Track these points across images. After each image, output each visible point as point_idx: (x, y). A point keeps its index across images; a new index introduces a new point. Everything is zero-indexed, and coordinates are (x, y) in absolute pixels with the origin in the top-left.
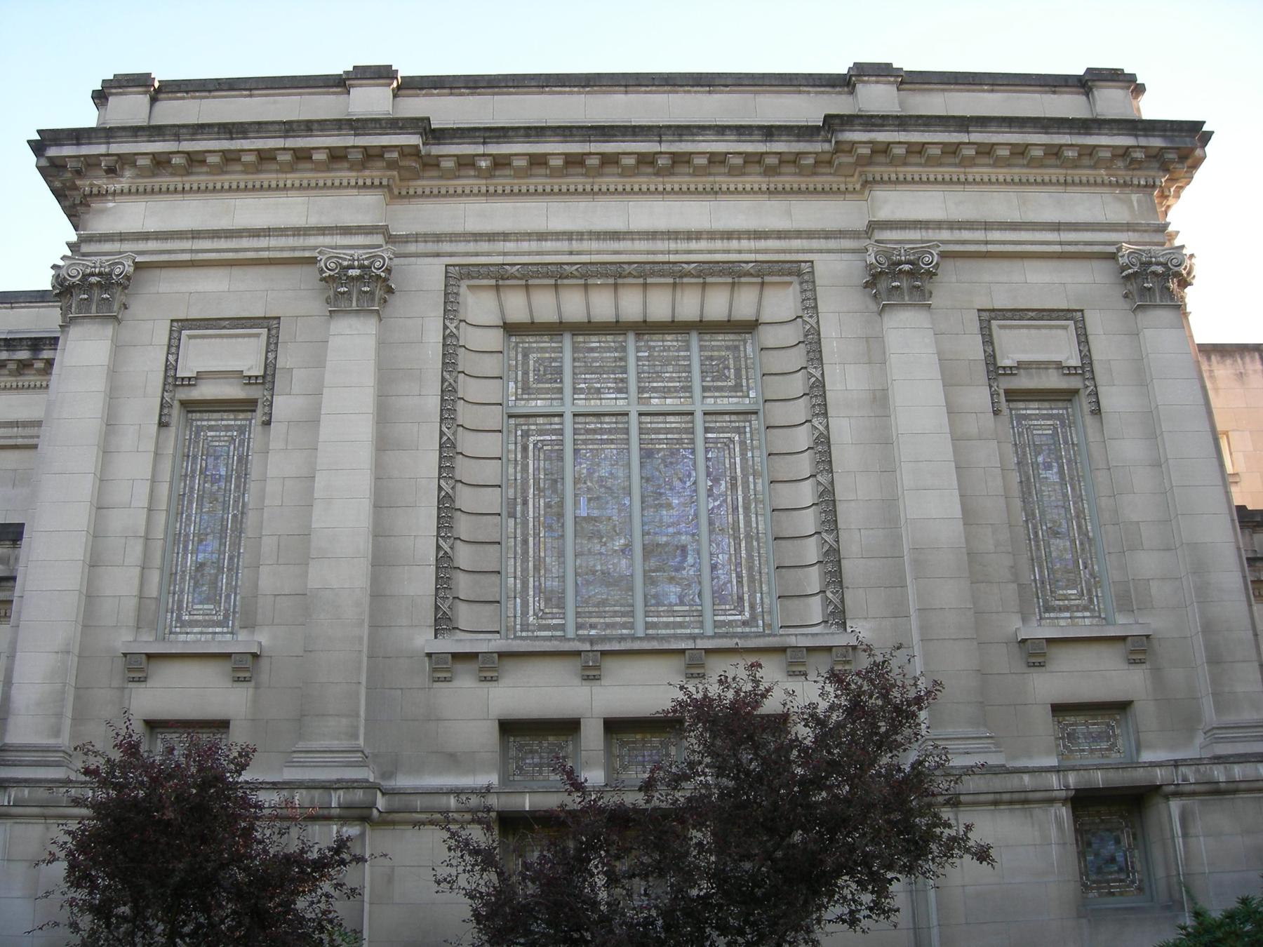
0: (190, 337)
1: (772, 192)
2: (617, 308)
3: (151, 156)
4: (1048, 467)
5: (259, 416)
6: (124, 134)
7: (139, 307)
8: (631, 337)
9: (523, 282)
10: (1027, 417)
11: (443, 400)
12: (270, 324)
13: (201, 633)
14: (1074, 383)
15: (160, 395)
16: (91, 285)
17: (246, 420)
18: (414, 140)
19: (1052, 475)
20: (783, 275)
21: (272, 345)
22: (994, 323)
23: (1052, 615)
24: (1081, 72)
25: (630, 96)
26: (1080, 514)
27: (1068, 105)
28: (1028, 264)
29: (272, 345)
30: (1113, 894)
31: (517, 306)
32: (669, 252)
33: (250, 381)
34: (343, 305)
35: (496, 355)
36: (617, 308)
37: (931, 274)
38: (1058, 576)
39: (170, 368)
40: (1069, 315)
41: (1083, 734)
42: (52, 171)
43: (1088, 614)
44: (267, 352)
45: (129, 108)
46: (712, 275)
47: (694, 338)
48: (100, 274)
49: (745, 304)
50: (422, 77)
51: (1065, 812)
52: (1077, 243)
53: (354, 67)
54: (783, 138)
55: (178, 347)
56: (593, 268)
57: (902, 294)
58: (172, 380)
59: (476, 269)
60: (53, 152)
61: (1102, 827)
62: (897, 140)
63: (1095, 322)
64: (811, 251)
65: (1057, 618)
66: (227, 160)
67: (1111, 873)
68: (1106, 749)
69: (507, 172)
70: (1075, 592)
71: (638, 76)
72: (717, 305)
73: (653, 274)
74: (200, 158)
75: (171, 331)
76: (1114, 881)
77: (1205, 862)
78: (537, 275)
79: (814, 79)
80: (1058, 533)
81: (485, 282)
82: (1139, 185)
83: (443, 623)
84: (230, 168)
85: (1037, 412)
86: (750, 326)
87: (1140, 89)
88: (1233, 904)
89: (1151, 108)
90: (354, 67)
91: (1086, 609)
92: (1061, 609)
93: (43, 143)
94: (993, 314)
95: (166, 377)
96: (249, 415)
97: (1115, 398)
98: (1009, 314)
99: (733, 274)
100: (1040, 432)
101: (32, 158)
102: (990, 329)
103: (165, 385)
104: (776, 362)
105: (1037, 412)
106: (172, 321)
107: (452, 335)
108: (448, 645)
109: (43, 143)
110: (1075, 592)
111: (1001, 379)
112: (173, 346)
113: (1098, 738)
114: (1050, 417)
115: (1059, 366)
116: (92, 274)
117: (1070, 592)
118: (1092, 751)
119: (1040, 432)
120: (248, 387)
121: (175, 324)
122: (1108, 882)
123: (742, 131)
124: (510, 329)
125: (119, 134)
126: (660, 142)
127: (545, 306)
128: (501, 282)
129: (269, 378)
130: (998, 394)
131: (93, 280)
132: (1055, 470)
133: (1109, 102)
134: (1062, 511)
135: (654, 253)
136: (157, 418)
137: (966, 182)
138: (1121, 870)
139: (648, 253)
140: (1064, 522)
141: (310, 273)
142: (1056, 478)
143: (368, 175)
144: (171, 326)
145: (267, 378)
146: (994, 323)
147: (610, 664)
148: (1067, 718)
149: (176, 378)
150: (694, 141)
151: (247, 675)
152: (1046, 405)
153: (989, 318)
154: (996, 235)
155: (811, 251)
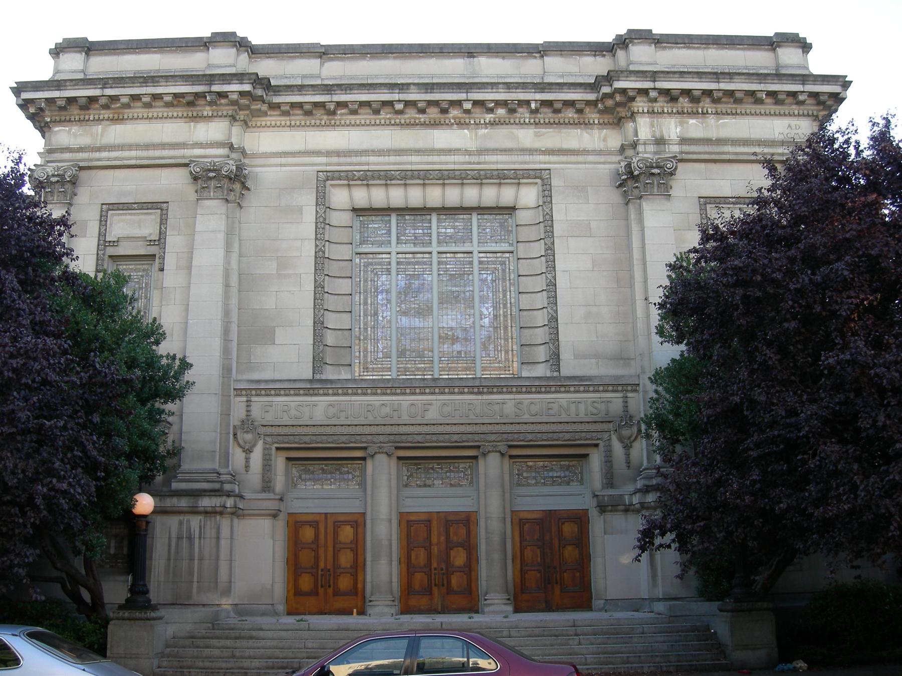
2: (424, 197)
6: (662, 75)
12: (159, 207)
14: (153, 250)
18: (247, 87)
21: (163, 221)
24: (771, 34)
27: (760, 60)
29: (163, 221)
31: (361, 196)
33: (151, 243)
34: (205, 194)
36: (424, 197)
39: (102, 235)
42: (24, 105)
45: (73, 63)
47: (475, 217)
48: (58, 175)
49: (507, 196)
54: (775, 82)
55: (106, 221)
57: (209, 192)
60: (25, 95)
63: (173, 212)
64: (550, 163)
66: (155, 99)
71: (173, 41)
72: (490, 195)
74: (224, 94)
75: (102, 211)
79: (727, 40)
81: (438, 182)
86: (511, 210)
87: (806, 47)
89: (818, 63)
93: (19, 89)
94: (111, 207)
95: (99, 240)
97: (170, 261)
99: (501, 177)
101: (13, 98)
103: (98, 245)
104: (524, 233)
109: (19, 89)
112: (103, 221)
121: (104, 206)
123: (700, 75)
124: (357, 211)
126: (803, 84)
127: (378, 196)
128: (389, 182)
129: (162, 241)
131: (54, 179)
133: (789, 56)
137: (736, 114)
139: (522, 163)
141: (183, 172)
144: (102, 208)
149: (105, 241)
155: (550, 163)
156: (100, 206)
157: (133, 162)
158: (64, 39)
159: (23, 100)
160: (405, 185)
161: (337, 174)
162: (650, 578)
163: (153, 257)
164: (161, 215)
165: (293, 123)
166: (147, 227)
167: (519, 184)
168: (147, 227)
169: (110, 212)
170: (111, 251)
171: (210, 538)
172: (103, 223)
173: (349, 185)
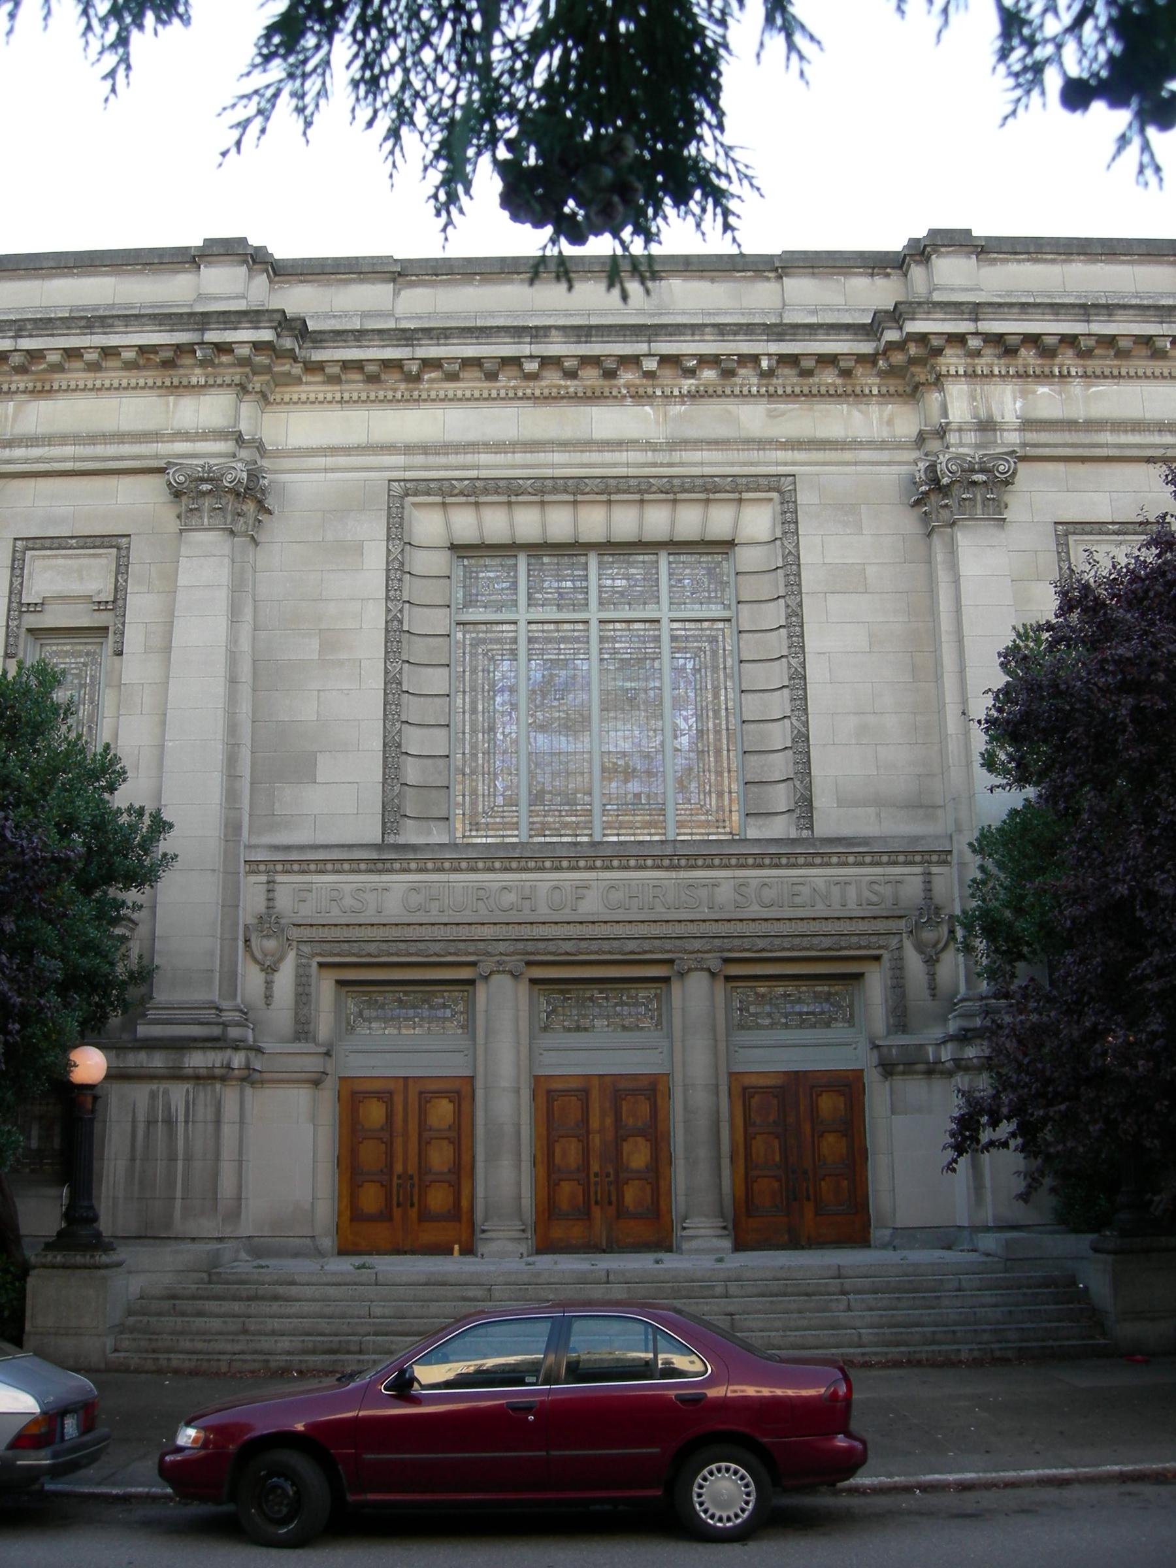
6: (990, 310)
8: (522, 562)
9: (736, 496)
15: (4, 624)
18: (266, 335)
21: (122, 569)
22: (1071, 538)
29: (122, 569)
33: (101, 606)
35: (442, 580)
37: (1007, 483)
39: (15, 593)
47: (663, 559)
50: (1086, 239)
53: (205, 240)
55: (22, 569)
59: (744, 480)
63: (139, 552)
73: (486, 491)
75: (14, 551)
77: (160, 1124)
78: (555, 490)
82: (957, 375)
86: (728, 545)
90: (205, 240)
94: (1071, 528)
95: (10, 602)
98: (98, 542)
102: (1067, 545)
103: (9, 611)
106: (16, 539)
111: (26, 616)
112: (17, 568)
120: (96, 613)
121: (19, 543)
123: (1056, 309)
124: (458, 549)
125: (1030, 311)
128: (513, 499)
129: (120, 603)
144: (14, 546)
145: (117, 603)
146: (1071, 538)
149: (21, 604)
150: (52, 335)
153: (1067, 530)
157: (69, 466)
161: (423, 485)
164: (118, 558)
167: (740, 500)
170: (31, 621)
172: (18, 572)
173: (444, 504)
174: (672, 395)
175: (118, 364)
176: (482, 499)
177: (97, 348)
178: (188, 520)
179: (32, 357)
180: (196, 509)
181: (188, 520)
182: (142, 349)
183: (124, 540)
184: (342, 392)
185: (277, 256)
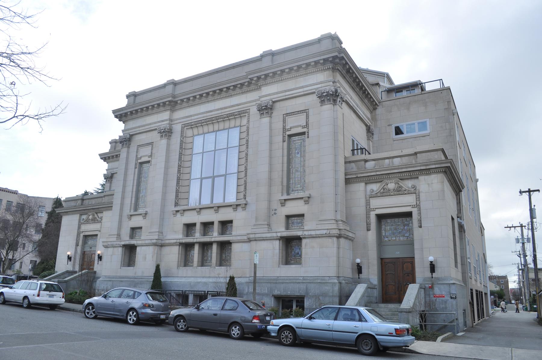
0: (288, 118)
1: (243, 93)
3: (297, 66)
4: (298, 153)
5: (306, 136)
7: (275, 113)
10: (295, 141)
11: (179, 156)
12: (151, 144)
13: (142, 209)
16: (263, 109)
17: (304, 137)
19: (299, 156)
20: (244, 113)
21: (307, 117)
23: (294, 192)
25: (218, 74)
26: (304, 166)
28: (297, 99)
29: (307, 117)
30: (297, 262)
32: (221, 113)
38: (296, 182)
40: (305, 111)
41: (296, 222)
43: (302, 191)
44: (306, 119)
46: (230, 117)
51: (120, 249)
52: (307, 91)
56: (208, 120)
57: (264, 115)
58: (284, 130)
61: (297, 245)
62: (302, 63)
63: (311, 112)
65: (294, 193)
67: (297, 257)
68: (301, 226)
69: (311, 67)
70: (299, 186)
76: (298, 259)
80: (298, 171)
83: (176, 204)
84: (309, 68)
85: (298, 139)
88: (434, 264)
91: (302, 190)
92: (296, 191)
96: (304, 136)
100: (297, 144)
103: (283, 131)
105: (298, 139)
106: (283, 115)
107: (182, 141)
108: (178, 208)
110: (299, 186)
111: (287, 132)
112: (284, 121)
113: (299, 223)
114: (301, 140)
115: (300, 126)
116: (263, 106)
117: (298, 186)
118: (297, 226)
119: (297, 144)
121: (284, 115)
122: (296, 259)
130: (285, 137)
131: (263, 108)
132: (300, 154)
134: (300, 165)
135: (212, 115)
136: (134, 167)
138: (299, 256)
140: (299, 168)
141: (156, 132)
142: (299, 156)
143: (309, 71)
145: (307, 126)
147: (203, 211)
148: (293, 218)
151: (284, 204)
152: (300, 136)
154: (141, 128)
156: (137, 146)
157: (302, 93)
158: (167, 81)
159: (249, 79)
160: (229, 119)
161: (231, 114)
162: (82, 254)
163: (303, 133)
164: (306, 114)
165: (307, 72)
166: (301, 120)
167: (241, 117)
168: (301, 120)
169: (286, 117)
170: (140, 161)
171: (161, 245)
172: (285, 122)
173: (197, 126)
174: (209, 101)
175: (278, 75)
176: (230, 118)
177: (264, 75)
178: (322, 102)
179: (283, 72)
180: (263, 113)
181: (322, 102)
182: (324, 59)
183: (308, 110)
184: (241, 91)
185: (176, 80)
